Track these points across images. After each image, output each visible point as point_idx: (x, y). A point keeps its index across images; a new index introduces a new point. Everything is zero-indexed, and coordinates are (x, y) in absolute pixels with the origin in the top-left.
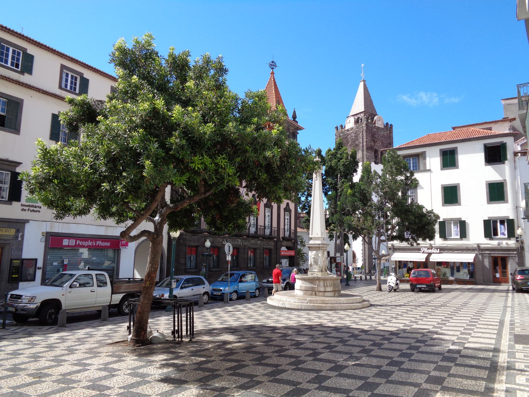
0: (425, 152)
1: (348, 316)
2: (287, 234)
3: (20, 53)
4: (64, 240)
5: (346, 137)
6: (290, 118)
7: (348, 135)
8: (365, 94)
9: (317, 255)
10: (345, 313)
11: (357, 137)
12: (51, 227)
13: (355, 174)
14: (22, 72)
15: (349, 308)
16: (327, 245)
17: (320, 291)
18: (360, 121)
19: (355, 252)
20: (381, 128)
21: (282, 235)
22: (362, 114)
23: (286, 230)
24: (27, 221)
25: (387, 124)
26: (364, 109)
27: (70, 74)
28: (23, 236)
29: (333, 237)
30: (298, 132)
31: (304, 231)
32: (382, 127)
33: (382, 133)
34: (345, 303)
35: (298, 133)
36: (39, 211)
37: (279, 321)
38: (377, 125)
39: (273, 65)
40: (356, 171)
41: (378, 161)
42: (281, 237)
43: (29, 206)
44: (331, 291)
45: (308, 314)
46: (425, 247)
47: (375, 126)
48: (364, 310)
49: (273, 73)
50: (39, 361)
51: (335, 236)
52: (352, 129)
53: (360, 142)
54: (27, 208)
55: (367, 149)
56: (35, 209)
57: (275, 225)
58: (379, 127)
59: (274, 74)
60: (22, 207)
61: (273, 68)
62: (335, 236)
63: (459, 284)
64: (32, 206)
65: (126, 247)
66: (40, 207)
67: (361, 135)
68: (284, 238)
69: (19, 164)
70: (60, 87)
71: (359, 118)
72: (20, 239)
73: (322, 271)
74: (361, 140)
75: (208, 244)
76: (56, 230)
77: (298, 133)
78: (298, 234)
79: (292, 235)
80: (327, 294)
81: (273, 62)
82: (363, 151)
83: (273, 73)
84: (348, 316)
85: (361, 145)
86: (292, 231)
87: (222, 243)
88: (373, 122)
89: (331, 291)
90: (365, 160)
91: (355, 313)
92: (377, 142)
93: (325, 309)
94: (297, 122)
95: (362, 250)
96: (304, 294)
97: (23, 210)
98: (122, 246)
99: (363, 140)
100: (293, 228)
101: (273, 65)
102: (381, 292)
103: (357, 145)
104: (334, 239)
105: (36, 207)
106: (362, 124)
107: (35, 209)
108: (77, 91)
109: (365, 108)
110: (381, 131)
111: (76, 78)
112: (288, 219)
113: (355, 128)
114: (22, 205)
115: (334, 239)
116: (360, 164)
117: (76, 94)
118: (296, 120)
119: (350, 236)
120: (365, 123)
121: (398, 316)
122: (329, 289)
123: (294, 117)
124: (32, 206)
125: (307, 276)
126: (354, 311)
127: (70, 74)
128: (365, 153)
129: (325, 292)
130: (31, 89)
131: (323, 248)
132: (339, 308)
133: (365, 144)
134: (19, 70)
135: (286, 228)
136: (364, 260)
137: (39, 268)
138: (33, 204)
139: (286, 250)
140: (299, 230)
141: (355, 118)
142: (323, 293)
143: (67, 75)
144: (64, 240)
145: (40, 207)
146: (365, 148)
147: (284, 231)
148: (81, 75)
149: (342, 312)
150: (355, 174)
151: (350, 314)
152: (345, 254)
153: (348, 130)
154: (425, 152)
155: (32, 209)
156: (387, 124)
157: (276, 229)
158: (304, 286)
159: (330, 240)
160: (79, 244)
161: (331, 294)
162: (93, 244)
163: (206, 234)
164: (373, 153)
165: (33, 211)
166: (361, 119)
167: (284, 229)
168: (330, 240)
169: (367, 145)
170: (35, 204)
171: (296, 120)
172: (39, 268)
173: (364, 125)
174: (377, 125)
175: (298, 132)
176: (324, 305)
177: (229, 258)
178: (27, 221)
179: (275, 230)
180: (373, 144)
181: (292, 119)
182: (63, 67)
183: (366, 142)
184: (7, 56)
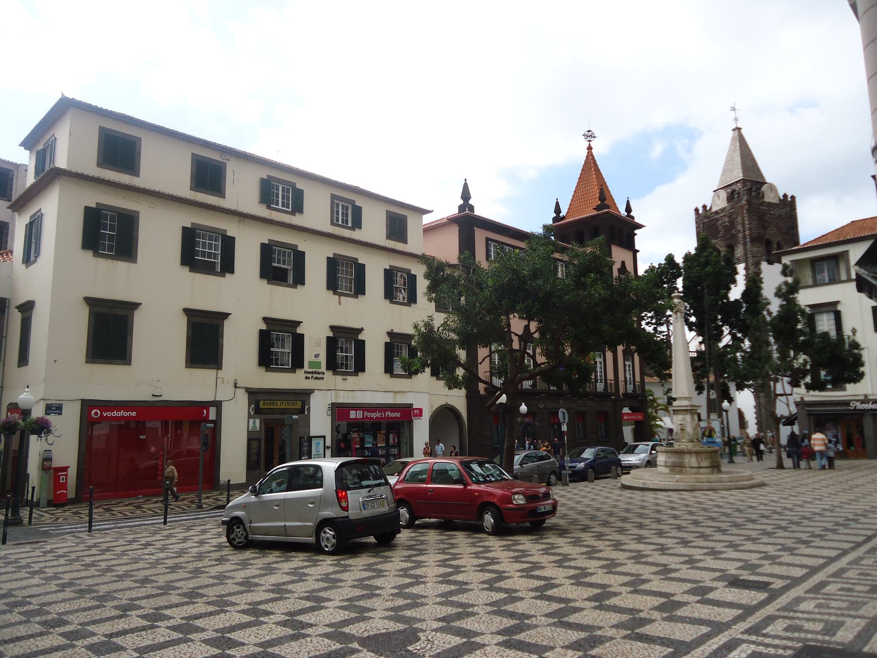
0: (847, 251)
1: (732, 495)
2: (630, 388)
3: (289, 189)
4: (351, 412)
5: (713, 224)
6: (623, 212)
7: (717, 220)
8: (741, 151)
9: (684, 419)
10: (728, 493)
11: (732, 223)
12: (336, 396)
13: (732, 286)
14: (293, 213)
15: (734, 487)
16: (697, 406)
17: (692, 467)
18: (736, 196)
19: (743, 410)
20: (775, 204)
21: (622, 390)
22: (739, 185)
23: (628, 383)
24: (312, 391)
25: (785, 196)
26: (742, 175)
27: (341, 204)
28: (309, 409)
29: (703, 389)
30: (636, 232)
31: (653, 381)
32: (776, 201)
33: (777, 212)
34: (727, 481)
35: (636, 234)
36: (323, 378)
37: (622, 520)
38: (766, 199)
39: (589, 136)
40: (734, 282)
41: (773, 258)
42: (621, 394)
43: (312, 373)
44: (707, 467)
45: (681, 494)
46: (857, 401)
47: (765, 202)
48: (754, 489)
49: (590, 148)
50: (216, 596)
51: (706, 387)
52: (723, 210)
53: (739, 231)
54: (310, 376)
55: (753, 240)
56: (319, 376)
57: (610, 376)
58: (770, 203)
59: (592, 149)
60: (306, 375)
61: (589, 141)
62: (706, 387)
63: (168, 430)
64: (316, 373)
65: (421, 418)
66: (324, 374)
67: (739, 219)
68: (626, 395)
69: (298, 323)
70: (332, 223)
71: (734, 191)
72: (306, 413)
73: (692, 441)
74: (740, 227)
75: (523, 408)
76: (341, 401)
77: (636, 234)
78: (647, 387)
79: (637, 389)
80: (702, 470)
81: (589, 131)
82: (745, 244)
83: (590, 148)
84: (732, 495)
85: (741, 235)
86: (637, 383)
87: (537, 406)
88: (760, 196)
89: (707, 467)
90: (750, 260)
91: (742, 493)
92: (768, 227)
93: (701, 489)
94: (633, 218)
95: (755, 407)
96: (671, 470)
97: (307, 378)
98: (414, 416)
99: (744, 225)
100: (638, 378)
101: (589, 136)
102: (783, 471)
103: (734, 236)
104: (705, 392)
105: (319, 373)
106: (740, 201)
107: (319, 376)
108: (350, 225)
109: (744, 173)
110: (775, 209)
111: (347, 207)
112: (629, 365)
113: (728, 209)
114: (306, 372)
115: (705, 392)
116: (741, 268)
117: (348, 228)
118: (632, 214)
119: (732, 386)
120: (745, 198)
121: (848, 523)
122: (704, 464)
123: (628, 209)
124: (316, 373)
125: (673, 448)
126: (741, 491)
127: (341, 204)
128: (749, 246)
129: (700, 467)
130: (304, 231)
131: (692, 411)
132: (720, 487)
133: (747, 232)
134: (290, 210)
135: (628, 376)
136: (759, 423)
137: (328, 448)
138: (316, 370)
139: (630, 412)
140: (647, 379)
141: (727, 193)
142: (694, 470)
143: (338, 205)
144: (351, 412)
145: (324, 374)
146: (748, 240)
147: (626, 384)
148: (352, 202)
149: (724, 492)
150: (732, 286)
151: (735, 494)
152: (724, 413)
153: (717, 213)
154: (847, 251)
155: (315, 376)
156: (785, 196)
157: (613, 382)
158: (670, 460)
159: (699, 394)
160: (366, 416)
161: (708, 470)
162: (382, 415)
163: (543, 395)
164: (764, 247)
165: (317, 378)
166: (739, 193)
167: (626, 381)
168: (699, 394)
169: (750, 235)
170: (318, 370)
171: (632, 214)
172: (328, 448)
173: (744, 202)
174: (766, 199)
175: (636, 232)
176: (699, 484)
177: (564, 428)
178: (312, 391)
179: (611, 384)
180: (762, 231)
181: (626, 214)
182: (333, 197)
183: (750, 229)
184: (277, 197)
